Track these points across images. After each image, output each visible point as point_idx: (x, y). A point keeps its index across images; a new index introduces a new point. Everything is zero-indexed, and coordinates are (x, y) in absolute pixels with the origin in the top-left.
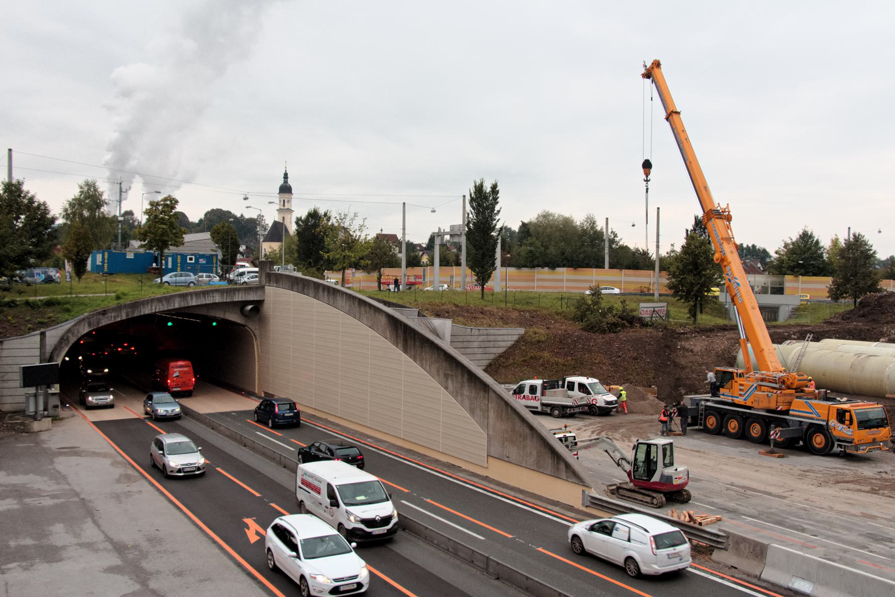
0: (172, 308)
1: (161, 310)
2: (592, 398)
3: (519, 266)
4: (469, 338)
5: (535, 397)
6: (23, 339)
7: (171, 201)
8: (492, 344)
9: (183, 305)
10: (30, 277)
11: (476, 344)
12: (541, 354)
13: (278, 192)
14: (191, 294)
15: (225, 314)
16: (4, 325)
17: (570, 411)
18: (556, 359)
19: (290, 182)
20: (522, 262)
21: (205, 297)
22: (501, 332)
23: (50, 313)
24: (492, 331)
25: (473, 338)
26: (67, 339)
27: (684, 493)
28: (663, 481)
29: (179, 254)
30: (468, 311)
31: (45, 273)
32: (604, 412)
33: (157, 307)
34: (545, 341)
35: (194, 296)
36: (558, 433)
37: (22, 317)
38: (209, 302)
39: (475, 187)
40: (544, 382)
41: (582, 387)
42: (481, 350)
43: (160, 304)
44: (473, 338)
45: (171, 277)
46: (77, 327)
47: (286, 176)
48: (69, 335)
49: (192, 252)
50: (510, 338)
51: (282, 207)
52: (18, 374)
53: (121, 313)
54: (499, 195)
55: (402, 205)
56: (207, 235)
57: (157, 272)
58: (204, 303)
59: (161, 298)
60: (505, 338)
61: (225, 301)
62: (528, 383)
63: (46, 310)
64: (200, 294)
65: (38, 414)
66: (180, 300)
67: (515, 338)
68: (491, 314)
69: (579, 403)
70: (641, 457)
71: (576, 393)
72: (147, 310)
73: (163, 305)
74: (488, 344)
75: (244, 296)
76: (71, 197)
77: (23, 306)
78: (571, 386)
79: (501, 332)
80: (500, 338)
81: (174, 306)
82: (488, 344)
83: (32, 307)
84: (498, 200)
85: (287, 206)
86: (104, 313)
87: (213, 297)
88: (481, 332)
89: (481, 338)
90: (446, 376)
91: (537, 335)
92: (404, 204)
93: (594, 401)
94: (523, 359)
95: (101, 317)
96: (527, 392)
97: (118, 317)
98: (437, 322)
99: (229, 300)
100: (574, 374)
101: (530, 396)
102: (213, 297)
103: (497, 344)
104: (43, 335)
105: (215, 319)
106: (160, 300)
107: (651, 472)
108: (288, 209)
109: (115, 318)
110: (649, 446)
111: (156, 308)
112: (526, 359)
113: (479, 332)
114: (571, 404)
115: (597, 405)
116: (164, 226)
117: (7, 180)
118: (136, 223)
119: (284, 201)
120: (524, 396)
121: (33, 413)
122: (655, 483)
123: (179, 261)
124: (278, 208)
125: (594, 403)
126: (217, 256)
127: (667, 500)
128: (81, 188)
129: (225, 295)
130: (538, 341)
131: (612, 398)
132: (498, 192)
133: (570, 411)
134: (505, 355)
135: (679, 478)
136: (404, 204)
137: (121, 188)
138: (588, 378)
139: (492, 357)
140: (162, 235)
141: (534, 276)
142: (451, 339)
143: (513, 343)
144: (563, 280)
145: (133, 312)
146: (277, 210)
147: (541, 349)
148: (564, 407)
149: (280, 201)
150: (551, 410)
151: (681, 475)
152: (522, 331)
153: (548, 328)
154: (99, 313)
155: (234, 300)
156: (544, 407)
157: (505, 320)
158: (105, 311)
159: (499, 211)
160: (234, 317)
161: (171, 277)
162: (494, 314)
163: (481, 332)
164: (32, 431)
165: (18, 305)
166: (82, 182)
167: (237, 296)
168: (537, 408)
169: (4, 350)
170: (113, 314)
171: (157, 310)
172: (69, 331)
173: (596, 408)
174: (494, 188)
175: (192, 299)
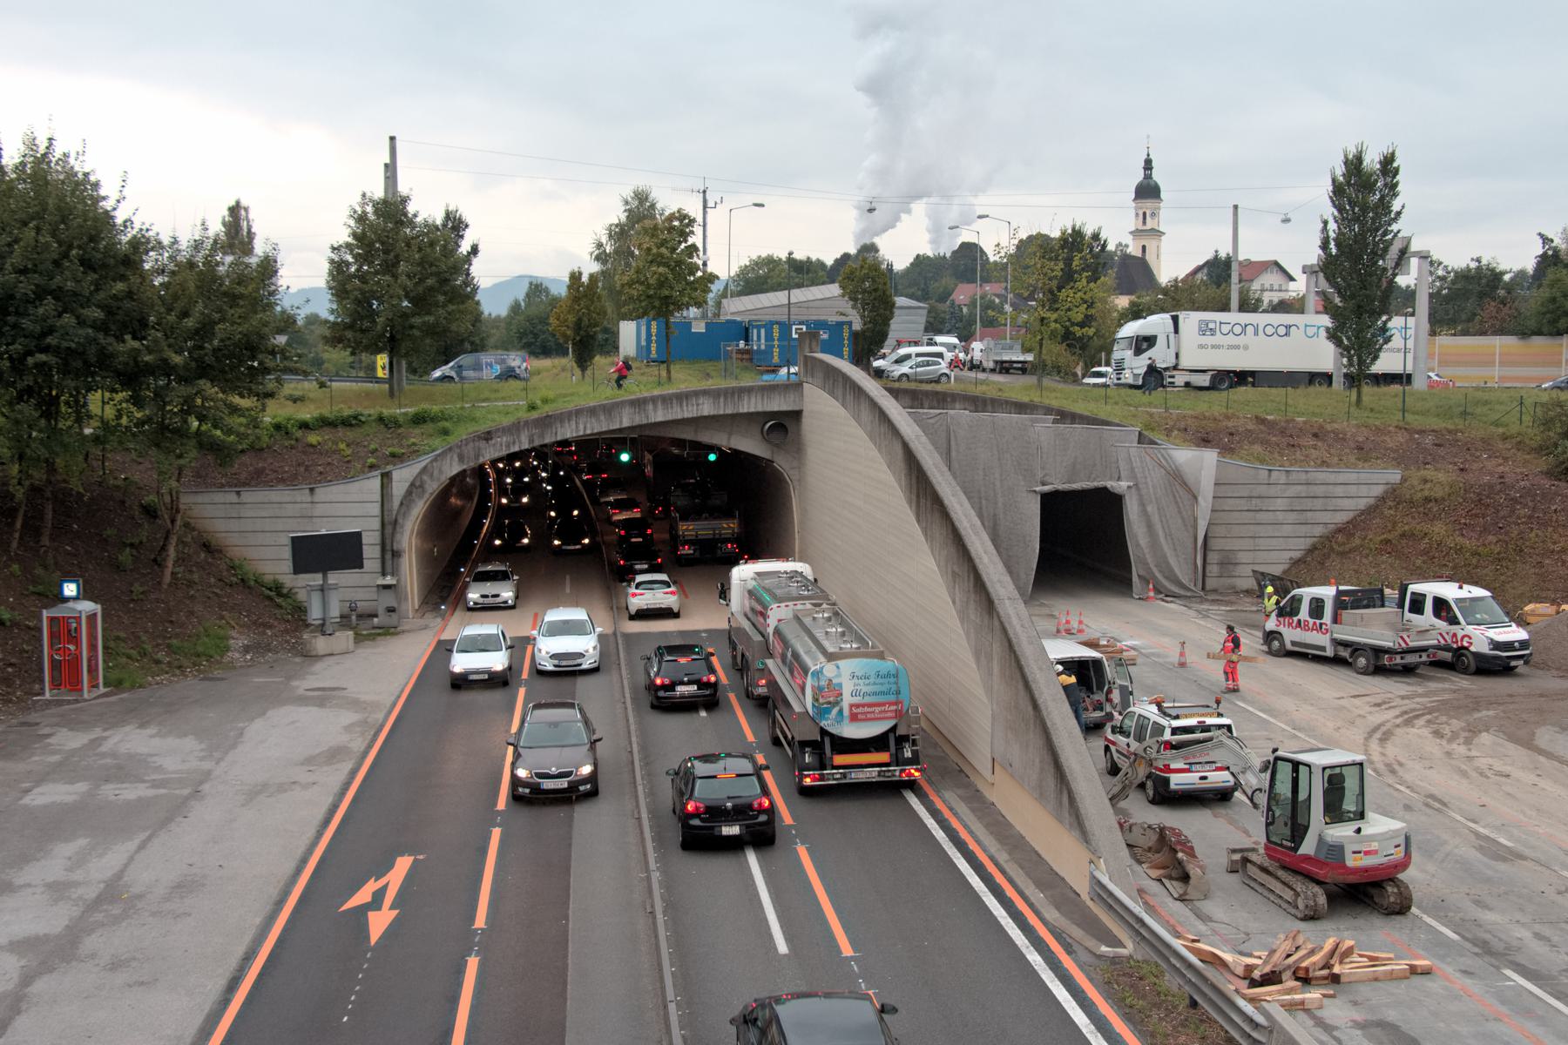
0: (617, 426)
1: (595, 431)
2: (1463, 633)
3: (1524, 333)
4: (1263, 490)
5: (1321, 624)
6: (351, 485)
7: (681, 221)
8: (1318, 504)
9: (639, 420)
10: (474, 369)
11: (1280, 504)
12: (1426, 527)
13: (1133, 196)
14: (654, 400)
15: (729, 439)
16: (330, 460)
17: (1391, 659)
18: (1459, 539)
19: (1157, 176)
20: (1532, 324)
21: (681, 406)
22: (1342, 478)
23: (415, 436)
24: (1322, 475)
25: (1273, 491)
26: (422, 486)
27: (1390, 889)
28: (1322, 856)
29: (777, 323)
30: (1283, 432)
31: (503, 362)
32: (1495, 665)
33: (588, 425)
34: (1443, 499)
35: (674, 401)
36: (1186, 716)
37: (366, 443)
38: (690, 416)
39: (1346, 162)
40: (1339, 593)
41: (1441, 606)
42: (1292, 517)
43: (593, 420)
44: (1273, 491)
45: (911, 368)
46: (439, 463)
47: (1148, 165)
48: (425, 477)
49: (804, 318)
50: (1364, 490)
51: (1141, 227)
52: (287, 548)
53: (519, 437)
54: (1398, 177)
55: (1232, 209)
56: (834, 290)
57: (745, 356)
58: (679, 417)
59: (595, 407)
60: (1353, 490)
61: (722, 412)
62: (1308, 594)
63: (411, 430)
64: (671, 399)
65: (328, 623)
66: (632, 410)
67: (1378, 491)
68: (1340, 437)
69: (1412, 644)
70: (1284, 788)
71: (1428, 618)
72: (568, 432)
73: (599, 421)
74: (1309, 504)
75: (760, 401)
76: (1045, 231)
77: (374, 424)
78: (1417, 605)
79: (1342, 478)
80: (1339, 491)
81: (621, 422)
82: (1309, 504)
83: (386, 425)
84: (1399, 188)
85: (1150, 224)
86: (488, 436)
87: (698, 405)
88: (1294, 477)
89: (1293, 491)
90: (954, 574)
91: (1428, 485)
92: (1236, 207)
93: (1466, 639)
94: (1383, 537)
95: (482, 444)
96: (1304, 613)
97: (514, 443)
98: (1184, 456)
99: (729, 411)
100: (1425, 577)
101: (1311, 621)
102: (698, 405)
103: (1333, 503)
104: (386, 477)
105: (712, 448)
106: (593, 411)
107: (1298, 831)
108: (1152, 229)
109: (508, 446)
110: (1296, 765)
111: (585, 428)
112: (1390, 536)
113: (1287, 477)
114: (1391, 644)
115: (1473, 649)
116: (661, 269)
117: (378, 192)
118: (884, 266)
119: (1144, 214)
120: (1299, 621)
121: (320, 622)
122: (1307, 858)
123: (776, 334)
124: (1133, 229)
125: (1465, 644)
126: (850, 324)
127: (1332, 898)
128: (627, 203)
129: (722, 400)
130: (1426, 498)
131: (1515, 634)
132: (1396, 171)
133: (1391, 659)
134: (1346, 530)
135: (1367, 853)
136: (1236, 207)
137: (705, 202)
138: (1461, 587)
139: (1318, 531)
140: (662, 284)
141: (1561, 354)
142: (1214, 491)
143: (1372, 501)
144: (1502, 364)
145: (542, 436)
146: (1131, 233)
147: (1431, 516)
148: (1378, 651)
149: (1137, 215)
150: (1352, 655)
151: (1374, 846)
152: (1394, 476)
153: (1462, 470)
154: (479, 438)
155: (741, 411)
156: (1340, 648)
157: (1365, 453)
158: (489, 433)
159: (1399, 213)
160: (749, 444)
161: (911, 368)
162: (1344, 439)
163: (1294, 477)
164: (314, 653)
165: (364, 423)
166: (628, 193)
167: (745, 402)
168: (1323, 649)
169: (318, 505)
170: (505, 439)
171: (588, 432)
172: (424, 470)
173: (1471, 658)
174: (1388, 163)
175: (655, 409)
